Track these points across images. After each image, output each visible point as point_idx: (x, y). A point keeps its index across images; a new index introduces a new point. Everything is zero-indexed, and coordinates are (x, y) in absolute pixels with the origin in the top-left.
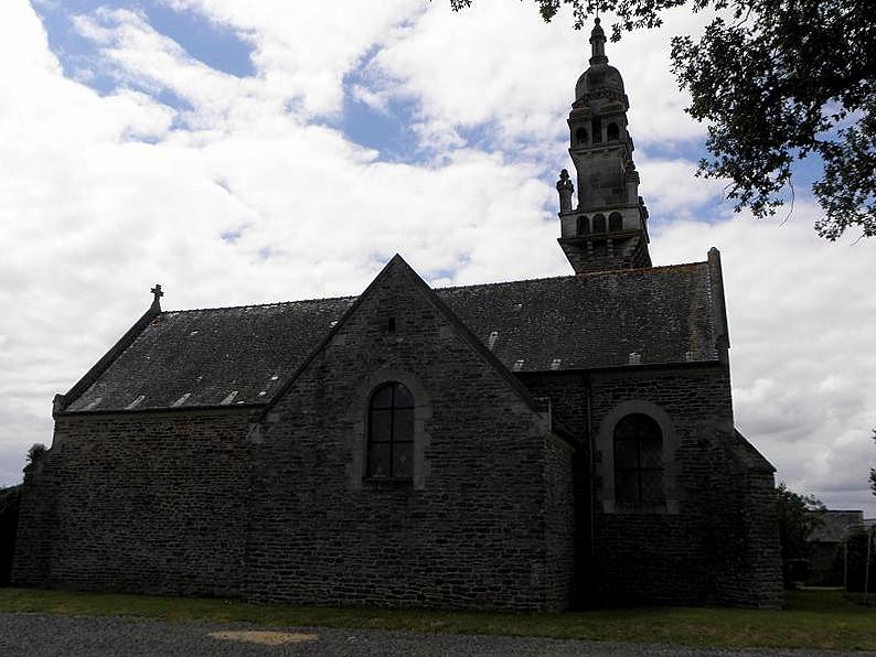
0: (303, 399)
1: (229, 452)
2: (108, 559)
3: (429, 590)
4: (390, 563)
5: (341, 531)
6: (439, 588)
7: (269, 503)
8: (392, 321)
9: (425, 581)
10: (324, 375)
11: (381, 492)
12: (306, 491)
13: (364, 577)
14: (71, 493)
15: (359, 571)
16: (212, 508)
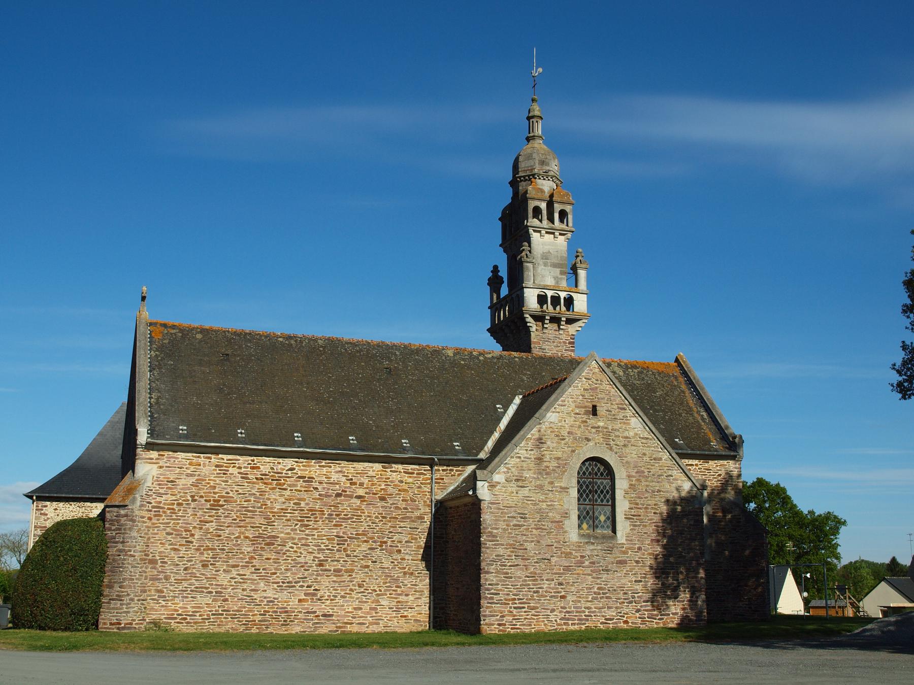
0: (525, 465)
1: (359, 497)
2: (226, 600)
3: (631, 617)
4: (601, 598)
5: (562, 574)
6: (638, 615)
7: (501, 551)
8: (594, 407)
11: (593, 544)
12: (532, 542)
14: (168, 530)
15: (579, 605)
16: (345, 550)
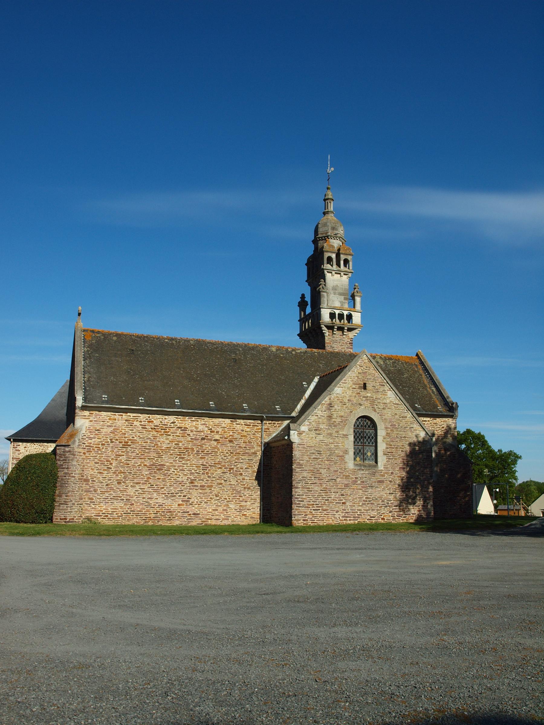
0: (320, 420)
4: (368, 504)
6: (390, 514)
7: (305, 474)
8: (365, 384)
9: (384, 512)
10: (331, 408)
11: (363, 470)
12: (325, 468)
13: (356, 511)
14: (96, 460)
15: (354, 508)
16: (207, 473)
